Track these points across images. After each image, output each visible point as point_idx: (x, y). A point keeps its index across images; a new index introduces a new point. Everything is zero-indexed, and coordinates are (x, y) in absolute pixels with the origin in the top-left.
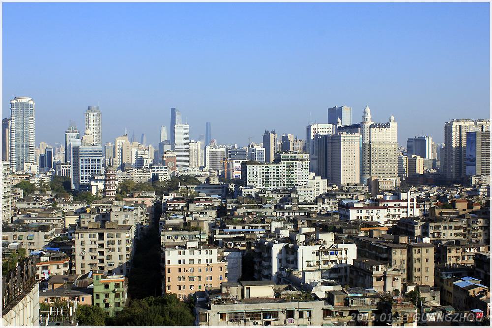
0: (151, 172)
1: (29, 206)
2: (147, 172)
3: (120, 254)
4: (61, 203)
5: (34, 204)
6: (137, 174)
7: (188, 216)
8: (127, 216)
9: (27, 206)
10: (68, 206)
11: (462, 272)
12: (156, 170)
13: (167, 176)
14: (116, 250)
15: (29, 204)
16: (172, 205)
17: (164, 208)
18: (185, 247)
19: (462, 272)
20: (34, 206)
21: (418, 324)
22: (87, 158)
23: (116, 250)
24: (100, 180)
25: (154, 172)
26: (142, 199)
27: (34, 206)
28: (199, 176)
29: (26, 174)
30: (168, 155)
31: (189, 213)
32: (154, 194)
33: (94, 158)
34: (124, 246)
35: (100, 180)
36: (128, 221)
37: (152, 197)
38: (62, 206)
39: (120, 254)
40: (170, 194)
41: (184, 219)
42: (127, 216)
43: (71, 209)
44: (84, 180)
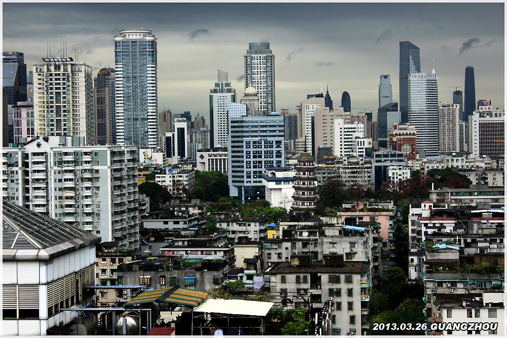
0: (375, 164)
1: (166, 226)
2: (366, 163)
3: (351, 313)
4: (221, 221)
5: (175, 223)
6: (348, 168)
7: (468, 245)
8: (352, 244)
9: (163, 227)
10: (235, 227)
11: (179, 220)
12: (383, 159)
13: (405, 171)
14: (345, 306)
15: (166, 223)
16: (437, 225)
17: (413, 231)
18: (480, 305)
19: (179, 220)
20: (176, 226)
21: (4, 198)
22: (257, 139)
23: (345, 306)
24: (287, 180)
25: (379, 164)
26: (371, 213)
27: (176, 226)
28: (465, 171)
29: (146, 168)
30: (401, 132)
31: (469, 240)
32: (391, 206)
33: (269, 139)
34: (357, 300)
35: (287, 180)
36: (356, 253)
37: (387, 210)
38: (224, 225)
39: (351, 313)
40: (423, 205)
41: (461, 251)
42: (352, 244)
43: (240, 232)
44: (252, 179)
